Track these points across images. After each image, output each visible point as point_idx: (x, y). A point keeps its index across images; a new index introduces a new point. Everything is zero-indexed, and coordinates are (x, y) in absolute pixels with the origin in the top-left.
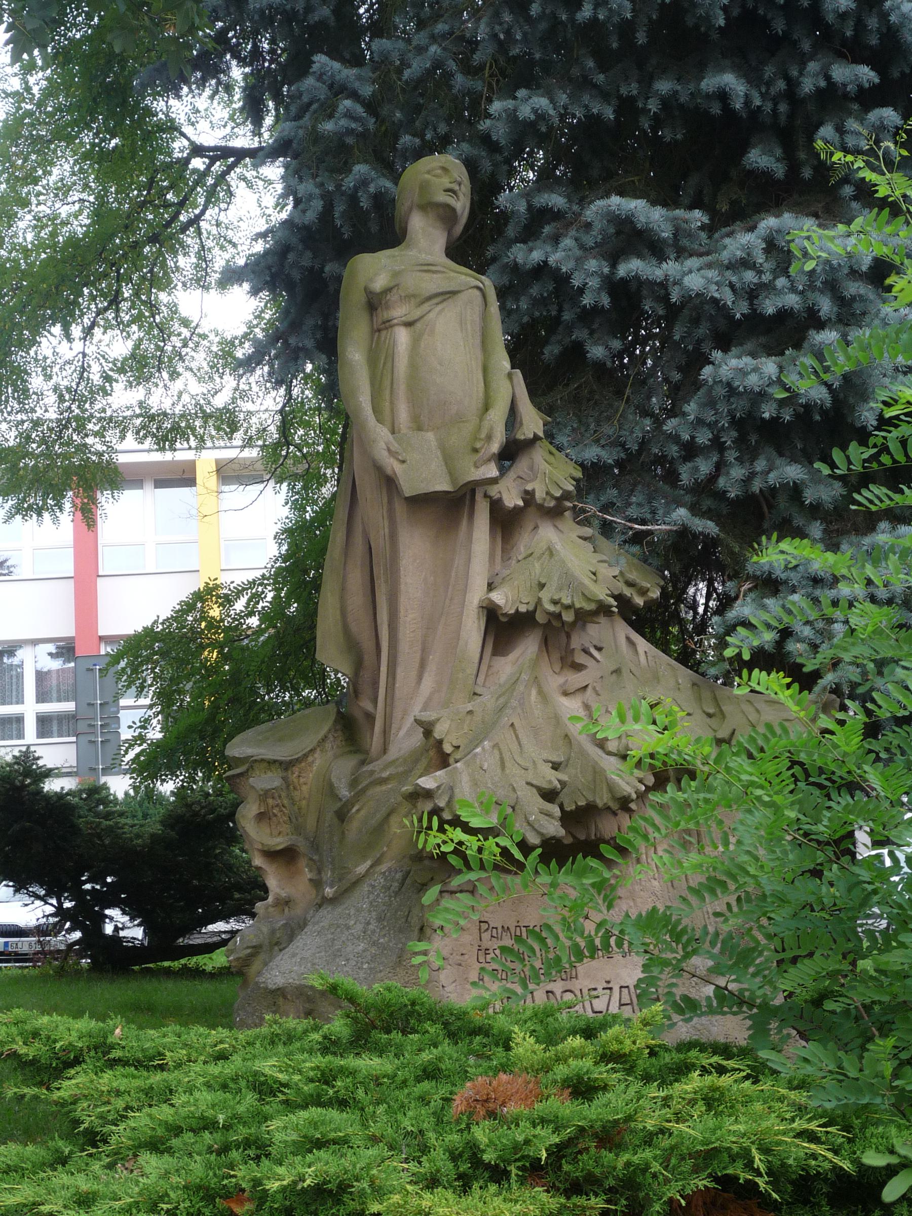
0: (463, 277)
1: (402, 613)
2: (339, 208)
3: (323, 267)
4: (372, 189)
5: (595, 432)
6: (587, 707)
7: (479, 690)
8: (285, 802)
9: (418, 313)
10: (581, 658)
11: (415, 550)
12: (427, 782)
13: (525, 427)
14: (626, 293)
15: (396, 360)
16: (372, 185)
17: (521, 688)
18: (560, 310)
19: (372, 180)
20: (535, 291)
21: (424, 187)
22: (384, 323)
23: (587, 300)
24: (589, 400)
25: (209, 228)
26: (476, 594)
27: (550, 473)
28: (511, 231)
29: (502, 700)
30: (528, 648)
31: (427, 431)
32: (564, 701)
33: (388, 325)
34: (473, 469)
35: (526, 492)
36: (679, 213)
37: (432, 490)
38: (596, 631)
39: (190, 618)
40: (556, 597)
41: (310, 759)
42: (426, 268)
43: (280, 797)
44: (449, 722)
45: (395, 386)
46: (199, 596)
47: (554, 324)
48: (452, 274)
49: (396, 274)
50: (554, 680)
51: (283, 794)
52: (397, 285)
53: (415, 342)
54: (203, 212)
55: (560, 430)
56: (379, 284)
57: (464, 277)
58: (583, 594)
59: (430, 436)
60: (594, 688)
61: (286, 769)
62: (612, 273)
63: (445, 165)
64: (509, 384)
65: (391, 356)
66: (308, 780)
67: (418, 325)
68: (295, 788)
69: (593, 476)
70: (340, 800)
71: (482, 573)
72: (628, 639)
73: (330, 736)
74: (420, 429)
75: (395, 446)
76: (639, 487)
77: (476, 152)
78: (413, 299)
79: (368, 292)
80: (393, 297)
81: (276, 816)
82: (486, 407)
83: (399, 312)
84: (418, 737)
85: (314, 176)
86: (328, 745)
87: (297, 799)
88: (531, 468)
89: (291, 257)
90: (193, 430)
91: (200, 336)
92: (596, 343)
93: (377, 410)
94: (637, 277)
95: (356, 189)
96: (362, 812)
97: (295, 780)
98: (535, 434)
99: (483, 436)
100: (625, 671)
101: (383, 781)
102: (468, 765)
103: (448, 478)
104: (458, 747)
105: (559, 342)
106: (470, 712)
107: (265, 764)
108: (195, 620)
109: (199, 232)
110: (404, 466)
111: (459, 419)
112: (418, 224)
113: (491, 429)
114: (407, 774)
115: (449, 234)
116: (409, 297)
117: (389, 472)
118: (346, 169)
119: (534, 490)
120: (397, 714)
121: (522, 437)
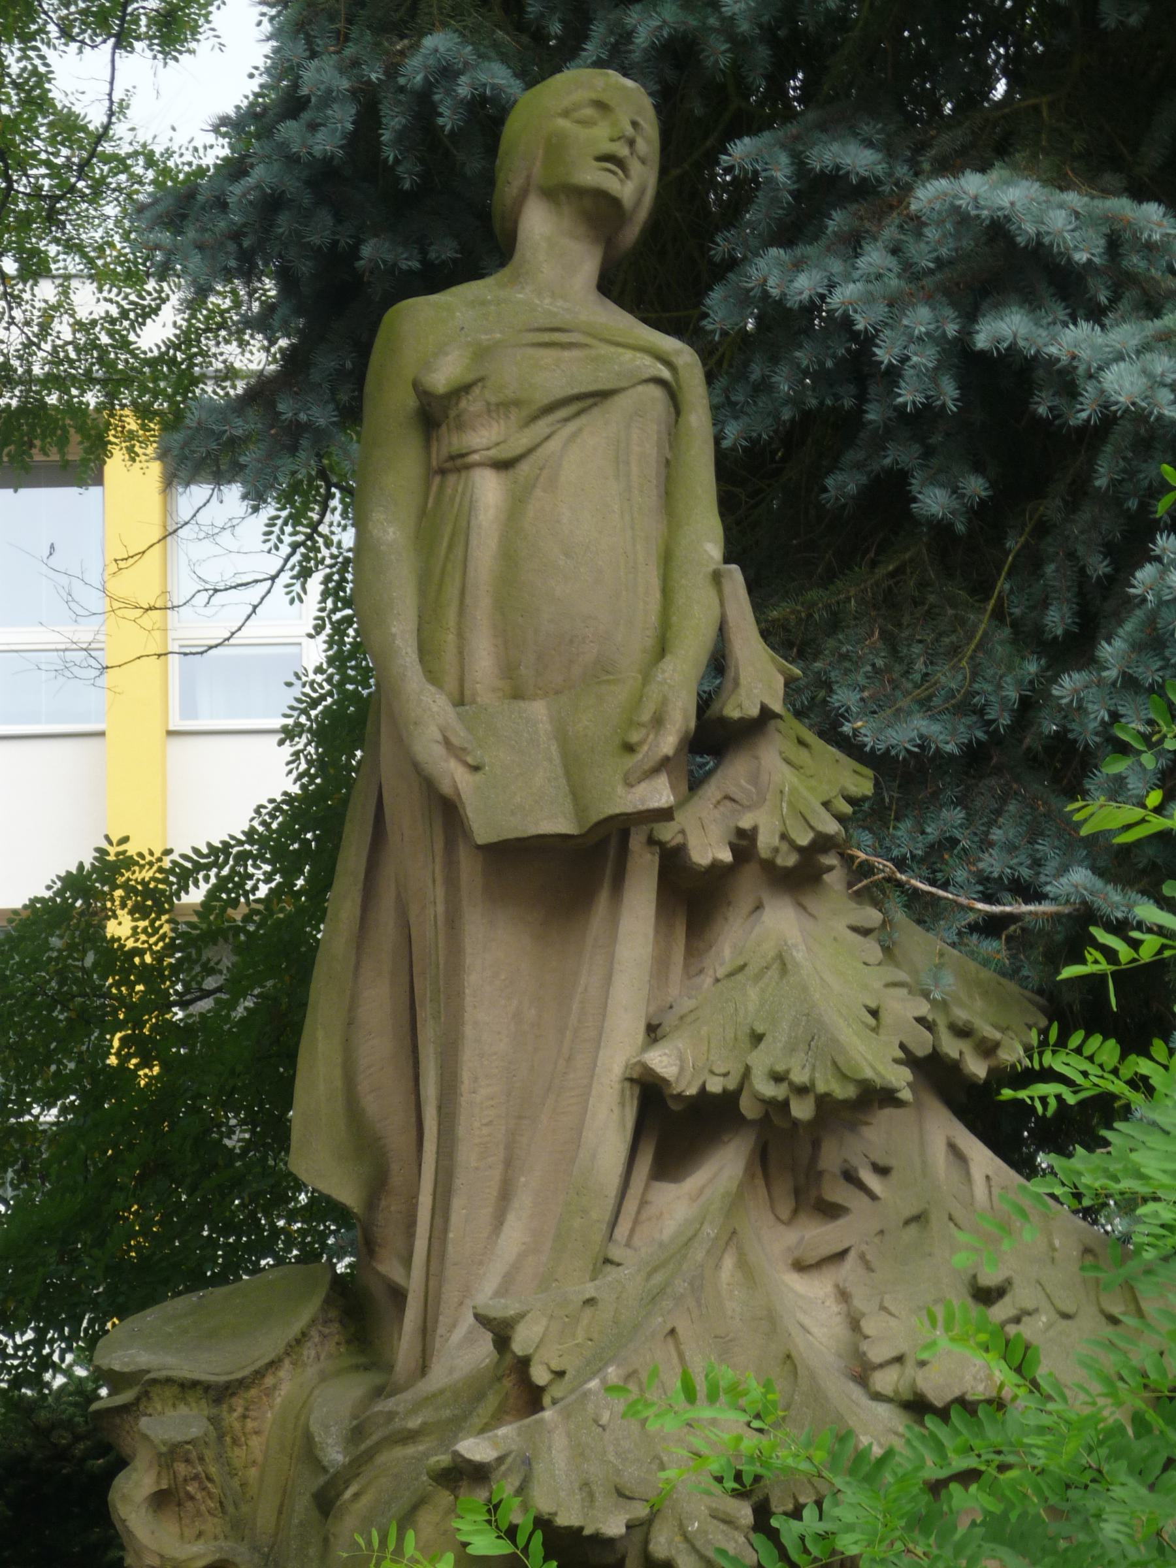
0: (628, 355)
1: (466, 1076)
2: (393, 121)
3: (359, 242)
4: (463, 89)
6: (844, 1295)
7: (615, 1253)
8: (213, 1470)
9: (521, 441)
10: (838, 1193)
11: (494, 962)
12: (476, 1448)
13: (742, 691)
14: (998, 381)
15: (474, 542)
16: (463, 79)
17: (698, 1254)
18: (862, 398)
21: (556, 147)
22: (452, 458)
23: (908, 395)
24: (916, 603)
26: (620, 1051)
27: (792, 789)
29: (658, 1278)
30: (723, 1168)
31: (534, 698)
32: (797, 1283)
33: (458, 464)
34: (620, 790)
35: (741, 833)
36: (1122, 206)
38: (880, 1134)
39: (55, 942)
40: (780, 1068)
41: (269, 1381)
42: (546, 337)
43: (201, 1459)
44: (544, 1322)
45: (468, 601)
47: (847, 425)
48: (605, 350)
49: (482, 353)
50: (776, 1239)
51: (209, 1454)
52: (481, 379)
55: (847, 672)
56: (444, 375)
57: (641, 349)
58: (835, 1063)
59: (538, 709)
60: (862, 1256)
61: (218, 1401)
62: (967, 333)
63: (604, 97)
64: (714, 595)
65: (463, 533)
66: (261, 1432)
67: (524, 467)
68: (235, 1442)
70: (325, 1470)
71: (627, 1004)
72: (952, 1147)
73: (313, 1332)
74: (517, 695)
75: (460, 736)
76: (1012, 807)
78: (514, 411)
79: (424, 394)
80: (471, 405)
81: (191, 1498)
82: (662, 649)
83: (484, 436)
84: (484, 1348)
85: (343, 39)
86: (308, 1352)
87: (237, 1463)
88: (755, 779)
89: (284, 223)
91: (106, 159)
92: (933, 481)
93: (426, 651)
94: (1013, 348)
95: (428, 88)
96: (365, 1500)
97: (237, 1425)
99: (646, 716)
100: (937, 1219)
101: (410, 1437)
102: (567, 1415)
104: (560, 1374)
106: (590, 1302)
107: (176, 1389)
108: (71, 947)
110: (478, 777)
111: (602, 671)
112: (539, 225)
113: (664, 702)
114: (456, 1426)
115: (609, 244)
116: (505, 406)
117: (446, 788)
119: (755, 829)
120: (451, 1294)
121: (736, 714)
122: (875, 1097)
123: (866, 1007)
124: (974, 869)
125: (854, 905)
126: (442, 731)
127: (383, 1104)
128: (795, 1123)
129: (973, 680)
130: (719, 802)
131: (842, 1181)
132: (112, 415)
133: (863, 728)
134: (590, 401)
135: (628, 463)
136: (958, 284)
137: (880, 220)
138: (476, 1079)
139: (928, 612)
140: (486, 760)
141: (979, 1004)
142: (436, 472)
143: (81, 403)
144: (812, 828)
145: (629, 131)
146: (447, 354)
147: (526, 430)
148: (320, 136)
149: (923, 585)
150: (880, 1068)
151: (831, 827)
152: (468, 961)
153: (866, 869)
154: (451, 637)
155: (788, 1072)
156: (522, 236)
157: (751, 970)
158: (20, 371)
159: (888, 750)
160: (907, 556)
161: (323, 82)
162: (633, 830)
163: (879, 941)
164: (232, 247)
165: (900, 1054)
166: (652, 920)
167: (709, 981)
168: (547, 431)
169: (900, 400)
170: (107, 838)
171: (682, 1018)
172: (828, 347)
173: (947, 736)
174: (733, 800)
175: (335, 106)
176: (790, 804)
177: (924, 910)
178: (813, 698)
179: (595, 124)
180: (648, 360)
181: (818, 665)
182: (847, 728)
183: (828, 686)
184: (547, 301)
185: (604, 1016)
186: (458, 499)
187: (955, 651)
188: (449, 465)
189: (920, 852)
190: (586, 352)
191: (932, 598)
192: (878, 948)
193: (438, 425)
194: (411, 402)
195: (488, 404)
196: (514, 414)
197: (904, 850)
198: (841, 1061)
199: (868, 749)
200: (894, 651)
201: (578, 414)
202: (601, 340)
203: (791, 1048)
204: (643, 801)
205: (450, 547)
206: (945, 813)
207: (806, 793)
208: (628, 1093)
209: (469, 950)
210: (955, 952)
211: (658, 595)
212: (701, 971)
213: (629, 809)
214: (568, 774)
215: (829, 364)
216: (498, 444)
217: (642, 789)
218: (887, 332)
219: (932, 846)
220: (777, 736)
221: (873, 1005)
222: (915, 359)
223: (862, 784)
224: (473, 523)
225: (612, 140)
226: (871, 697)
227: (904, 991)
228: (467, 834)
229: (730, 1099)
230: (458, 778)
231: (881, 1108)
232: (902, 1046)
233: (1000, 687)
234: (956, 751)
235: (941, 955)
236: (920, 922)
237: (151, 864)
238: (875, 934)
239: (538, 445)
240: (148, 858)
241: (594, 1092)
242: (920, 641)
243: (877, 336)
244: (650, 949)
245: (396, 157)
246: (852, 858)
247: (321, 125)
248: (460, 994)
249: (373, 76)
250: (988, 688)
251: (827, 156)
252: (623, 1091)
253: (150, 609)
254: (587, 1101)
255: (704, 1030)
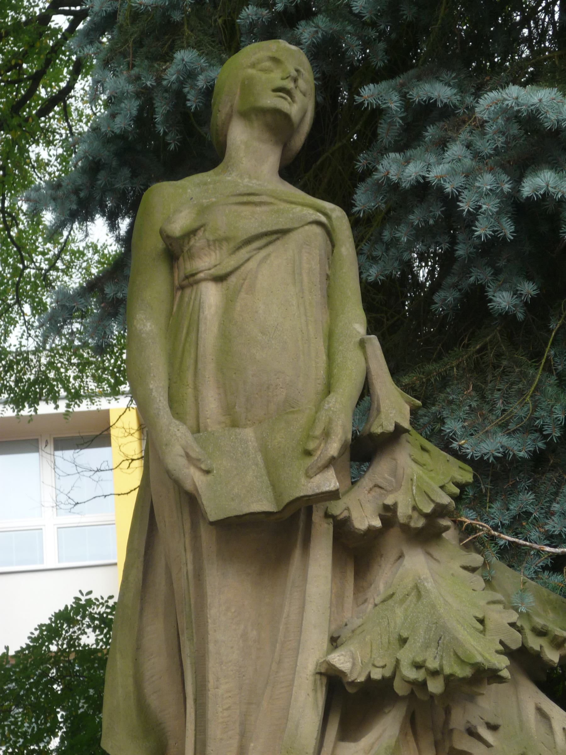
0: (299, 208)
2: (161, 109)
5: (504, 410)
9: (231, 263)
13: (383, 416)
15: (202, 328)
16: (201, 77)
19: (203, 70)
20: (415, 218)
21: (247, 87)
22: (187, 277)
23: (482, 230)
24: (495, 367)
25: (80, 105)
26: (312, 654)
27: (417, 477)
28: (386, 132)
31: (245, 426)
34: (303, 480)
35: (386, 508)
37: (246, 510)
38: (490, 702)
40: (419, 659)
42: (245, 199)
45: (200, 366)
46: (65, 617)
48: (283, 205)
49: (203, 210)
52: (203, 226)
53: (229, 302)
54: (70, 87)
55: (453, 411)
56: (179, 225)
57: (302, 207)
58: (456, 654)
59: (249, 433)
63: (277, 55)
64: (362, 355)
67: (233, 279)
69: (492, 477)
72: (539, 710)
74: (234, 424)
75: (196, 451)
77: (336, 27)
78: (225, 244)
79: (166, 237)
80: (198, 242)
82: (328, 389)
83: (206, 261)
88: (394, 473)
90: (65, 382)
91: (73, 253)
92: (500, 288)
93: (174, 401)
94: (546, 195)
95: (181, 83)
98: (397, 426)
99: (318, 432)
103: (269, 493)
105: (455, 286)
109: (66, 114)
110: (210, 477)
112: (241, 138)
113: (330, 421)
115: (285, 147)
116: (219, 241)
117: (188, 486)
118: (167, 57)
119: (395, 505)
121: (379, 431)
122: (485, 675)
123: (476, 617)
124: (542, 530)
125: (464, 553)
126: (184, 448)
127: (160, 700)
128: (432, 696)
129: (534, 410)
130: (371, 489)
131: (466, 735)
132: (82, 381)
133: (467, 445)
134: (274, 237)
135: (301, 274)
136: (509, 162)
137: (457, 130)
138: (218, 680)
139: (503, 372)
140: (214, 466)
141: (551, 615)
142: (178, 289)
143: (66, 376)
144: (433, 501)
145: (294, 73)
146: (181, 212)
147: (233, 256)
148: (118, 119)
149: (498, 356)
150: (487, 656)
151: (446, 500)
152: (209, 601)
153: (471, 529)
154: (190, 391)
155: (425, 661)
156: (229, 143)
157: (397, 597)
158: (35, 361)
159: (482, 457)
160: (488, 339)
161: (118, 89)
162: (314, 506)
163: (483, 576)
164: (74, 198)
165: (501, 648)
166: (330, 567)
167: (370, 606)
168: (247, 256)
169: (477, 233)
170: (80, 591)
171: (353, 631)
172: (431, 212)
173: (521, 447)
174: (380, 487)
175: (126, 101)
176: (418, 487)
177: (512, 555)
178: (433, 430)
179: (272, 71)
180: (311, 211)
181: (434, 409)
182: (455, 445)
183: (442, 421)
184: (246, 180)
185: (301, 632)
186: (192, 303)
187: (521, 393)
188: (185, 282)
189: (507, 522)
190: (271, 207)
191: (505, 363)
192: (482, 580)
193: (177, 259)
194: (160, 245)
195: (208, 241)
196: (225, 247)
197: (496, 521)
198: (460, 653)
199: (469, 456)
200: (483, 397)
201: (267, 245)
202: (280, 200)
203: (426, 646)
204: (318, 488)
205: (188, 333)
206: (521, 496)
207: (427, 479)
208: (318, 683)
209: (209, 593)
210: (533, 582)
211: (324, 357)
212: (365, 601)
213: (310, 493)
214: (269, 474)
215: (431, 222)
216: (215, 266)
217: (318, 479)
218: (466, 192)
219: (514, 518)
220: (408, 445)
221: (480, 616)
222: (484, 207)
223: (466, 475)
224: (201, 316)
225: (283, 79)
226: (469, 426)
227: (501, 607)
228: (204, 516)
229: (387, 683)
230: (196, 479)
231: (489, 683)
232: (501, 642)
233: (551, 412)
234: (526, 456)
235: (524, 583)
236: (511, 566)
237: (102, 604)
238: (480, 570)
239: (242, 265)
240: (101, 601)
241: (296, 683)
242: (499, 390)
243: (460, 195)
244: (329, 586)
245: (164, 131)
246: (462, 523)
247: (117, 114)
248: (206, 624)
249: (149, 83)
250: (544, 413)
251: (421, 93)
252: (315, 681)
253: (98, 471)
254: (292, 689)
255: (368, 638)
